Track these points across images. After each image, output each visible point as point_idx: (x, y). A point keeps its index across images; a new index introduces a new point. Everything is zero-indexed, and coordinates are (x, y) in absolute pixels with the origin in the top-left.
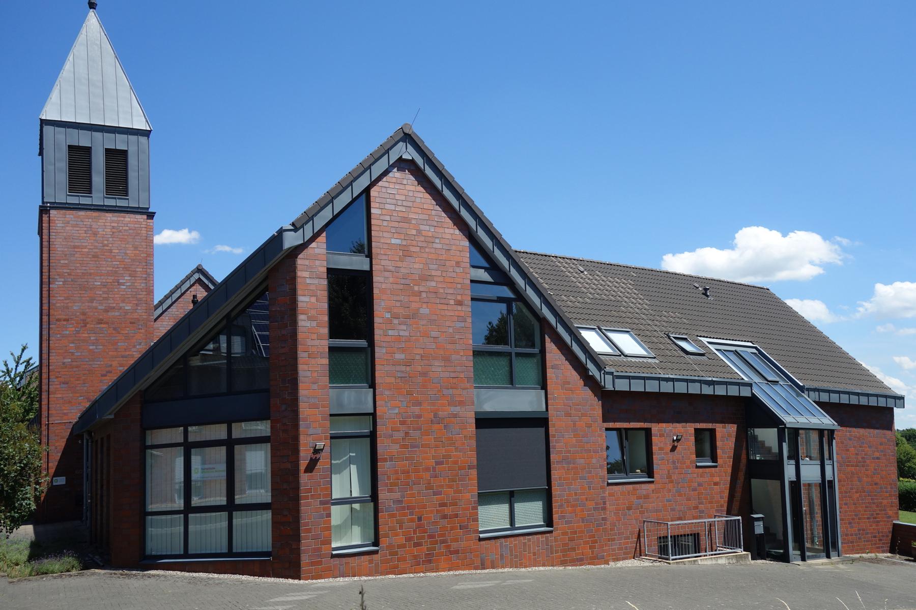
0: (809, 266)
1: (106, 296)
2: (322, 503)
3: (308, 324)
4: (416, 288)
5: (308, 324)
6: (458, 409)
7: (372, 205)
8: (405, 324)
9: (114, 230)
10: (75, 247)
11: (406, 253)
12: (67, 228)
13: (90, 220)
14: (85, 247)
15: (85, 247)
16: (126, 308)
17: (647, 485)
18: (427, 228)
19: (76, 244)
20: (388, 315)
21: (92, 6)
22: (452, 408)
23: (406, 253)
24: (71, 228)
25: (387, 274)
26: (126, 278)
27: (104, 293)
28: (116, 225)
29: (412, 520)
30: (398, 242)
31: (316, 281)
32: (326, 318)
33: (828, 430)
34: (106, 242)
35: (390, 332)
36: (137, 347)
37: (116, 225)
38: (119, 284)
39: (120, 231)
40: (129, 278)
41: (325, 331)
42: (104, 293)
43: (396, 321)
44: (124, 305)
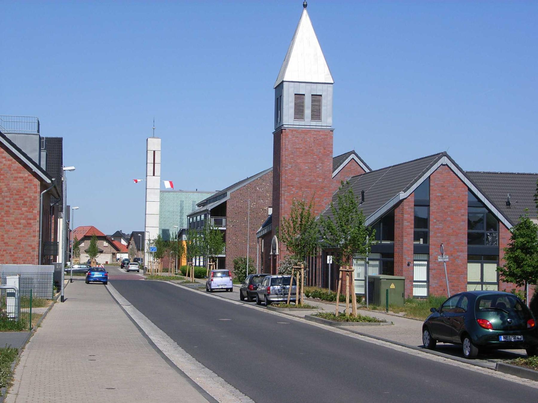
0: (263, 296)
1: (310, 174)
2: (410, 281)
3: (407, 224)
4: (446, 211)
5: (407, 224)
6: (460, 253)
7: (431, 182)
8: (441, 223)
9: (314, 139)
10: (297, 148)
11: (442, 198)
12: (294, 139)
13: (304, 134)
14: (301, 148)
15: (301, 148)
16: (319, 180)
17: (145, 207)
18: (451, 188)
19: (297, 147)
20: (435, 221)
21: (305, 6)
22: (458, 253)
23: (442, 198)
24: (295, 139)
25: (435, 206)
26: (320, 165)
27: (309, 172)
28: (315, 136)
29: (441, 290)
30: (440, 194)
31: (410, 209)
32: (413, 222)
33: (394, 260)
34: (311, 146)
35: (435, 226)
36: (324, 201)
37: (315, 136)
38: (317, 168)
39: (317, 140)
40: (321, 165)
41: (413, 226)
42: (309, 172)
43: (438, 222)
44: (319, 179)
